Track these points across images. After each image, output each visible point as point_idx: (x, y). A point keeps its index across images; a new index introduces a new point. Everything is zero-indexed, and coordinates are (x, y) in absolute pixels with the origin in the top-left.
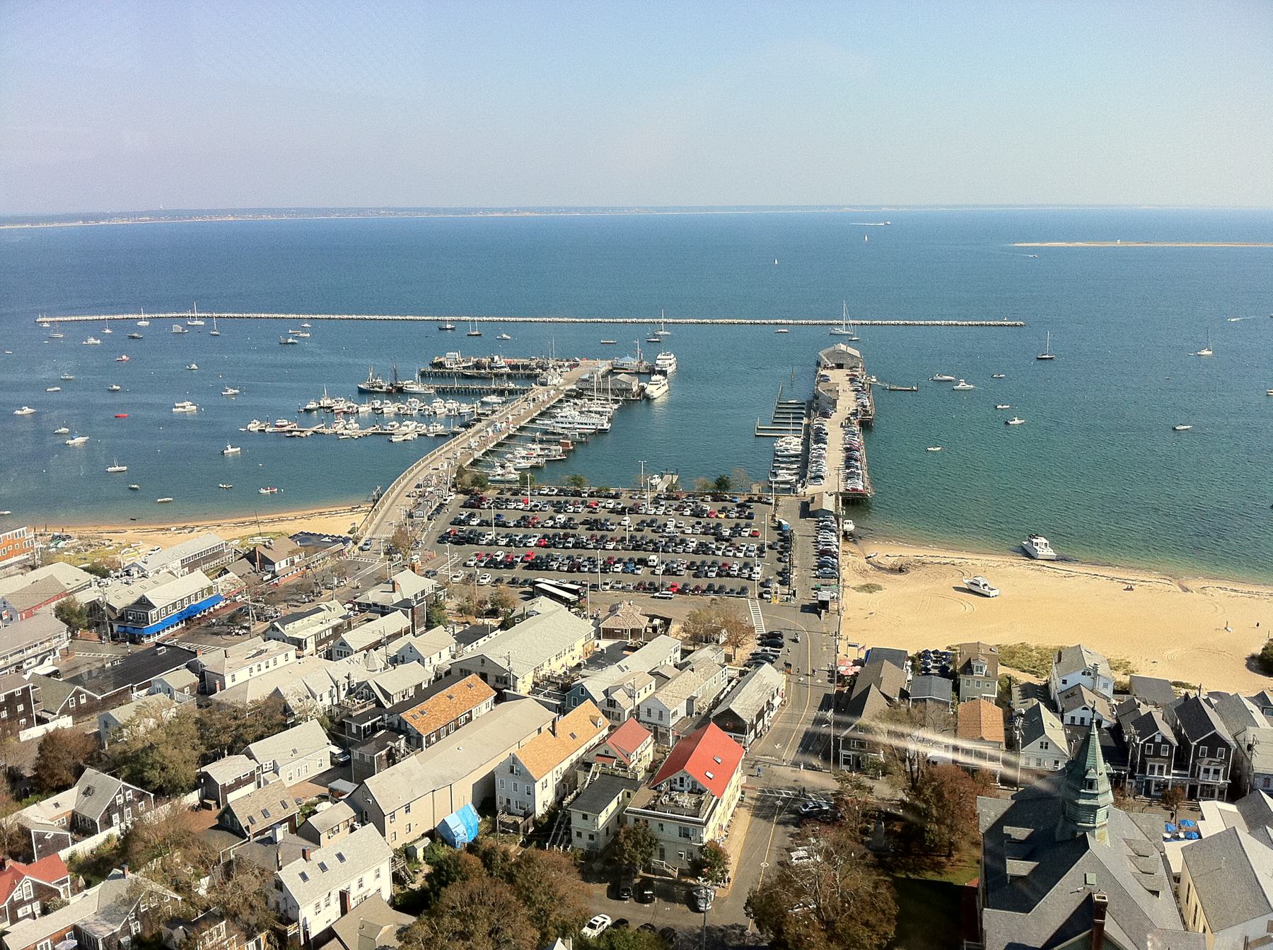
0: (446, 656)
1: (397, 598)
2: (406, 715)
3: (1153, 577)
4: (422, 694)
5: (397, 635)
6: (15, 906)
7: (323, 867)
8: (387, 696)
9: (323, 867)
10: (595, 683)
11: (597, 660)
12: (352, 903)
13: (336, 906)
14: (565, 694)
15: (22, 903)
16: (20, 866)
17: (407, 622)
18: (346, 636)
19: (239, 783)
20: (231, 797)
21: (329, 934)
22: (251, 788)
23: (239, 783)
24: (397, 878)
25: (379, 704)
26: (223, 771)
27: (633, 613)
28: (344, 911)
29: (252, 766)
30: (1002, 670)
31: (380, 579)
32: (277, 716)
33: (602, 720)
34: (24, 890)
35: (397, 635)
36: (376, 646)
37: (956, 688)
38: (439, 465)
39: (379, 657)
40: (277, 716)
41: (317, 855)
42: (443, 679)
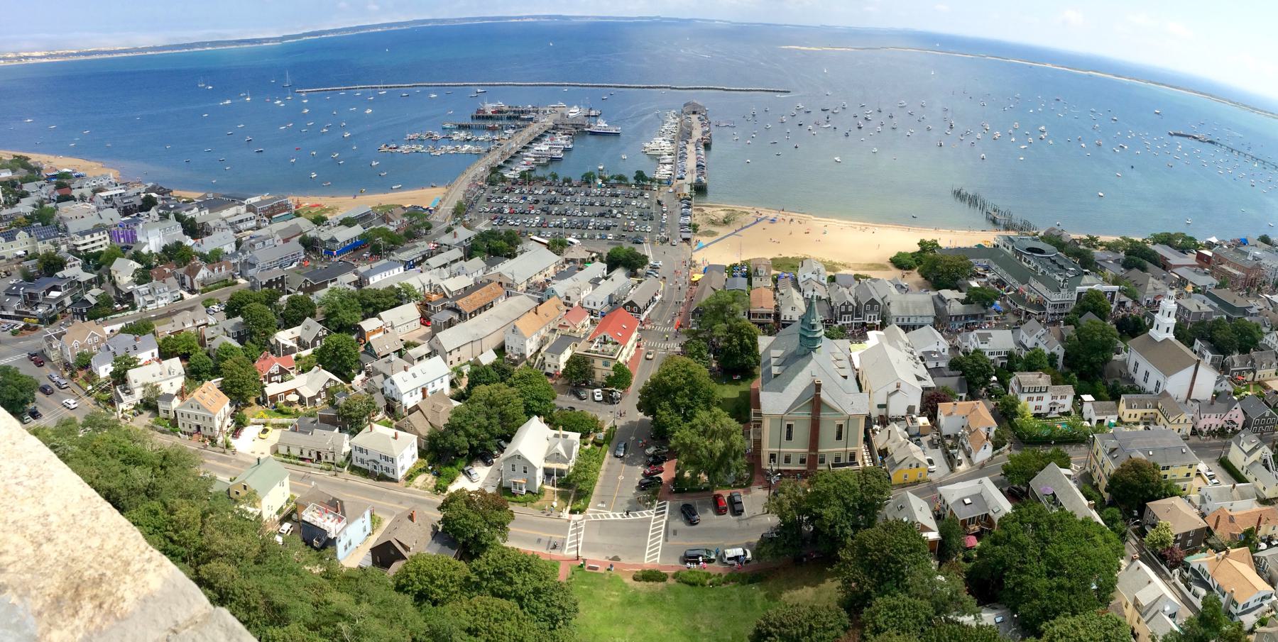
0: (481, 273)
1: (456, 241)
2: (459, 302)
3: (843, 223)
4: (467, 291)
5: (456, 261)
6: (271, 375)
7: (414, 376)
8: (407, 549)
9: (414, 376)
10: (561, 287)
11: (560, 276)
12: (428, 393)
13: (420, 395)
14: (541, 291)
15: (273, 375)
16: (273, 357)
17: (462, 254)
18: (429, 261)
19: (374, 332)
20: (371, 338)
21: (417, 408)
22: (381, 334)
23: (374, 332)
24: (452, 384)
25: (445, 296)
26: (368, 325)
27: (578, 252)
28: (424, 397)
29: (380, 323)
30: (773, 272)
31: (449, 230)
32: (396, 297)
33: (564, 308)
34: (275, 369)
35: (456, 261)
36: (444, 266)
37: (750, 283)
38: (480, 169)
39: (445, 272)
40: (396, 297)
41: (411, 370)
42: (478, 285)
